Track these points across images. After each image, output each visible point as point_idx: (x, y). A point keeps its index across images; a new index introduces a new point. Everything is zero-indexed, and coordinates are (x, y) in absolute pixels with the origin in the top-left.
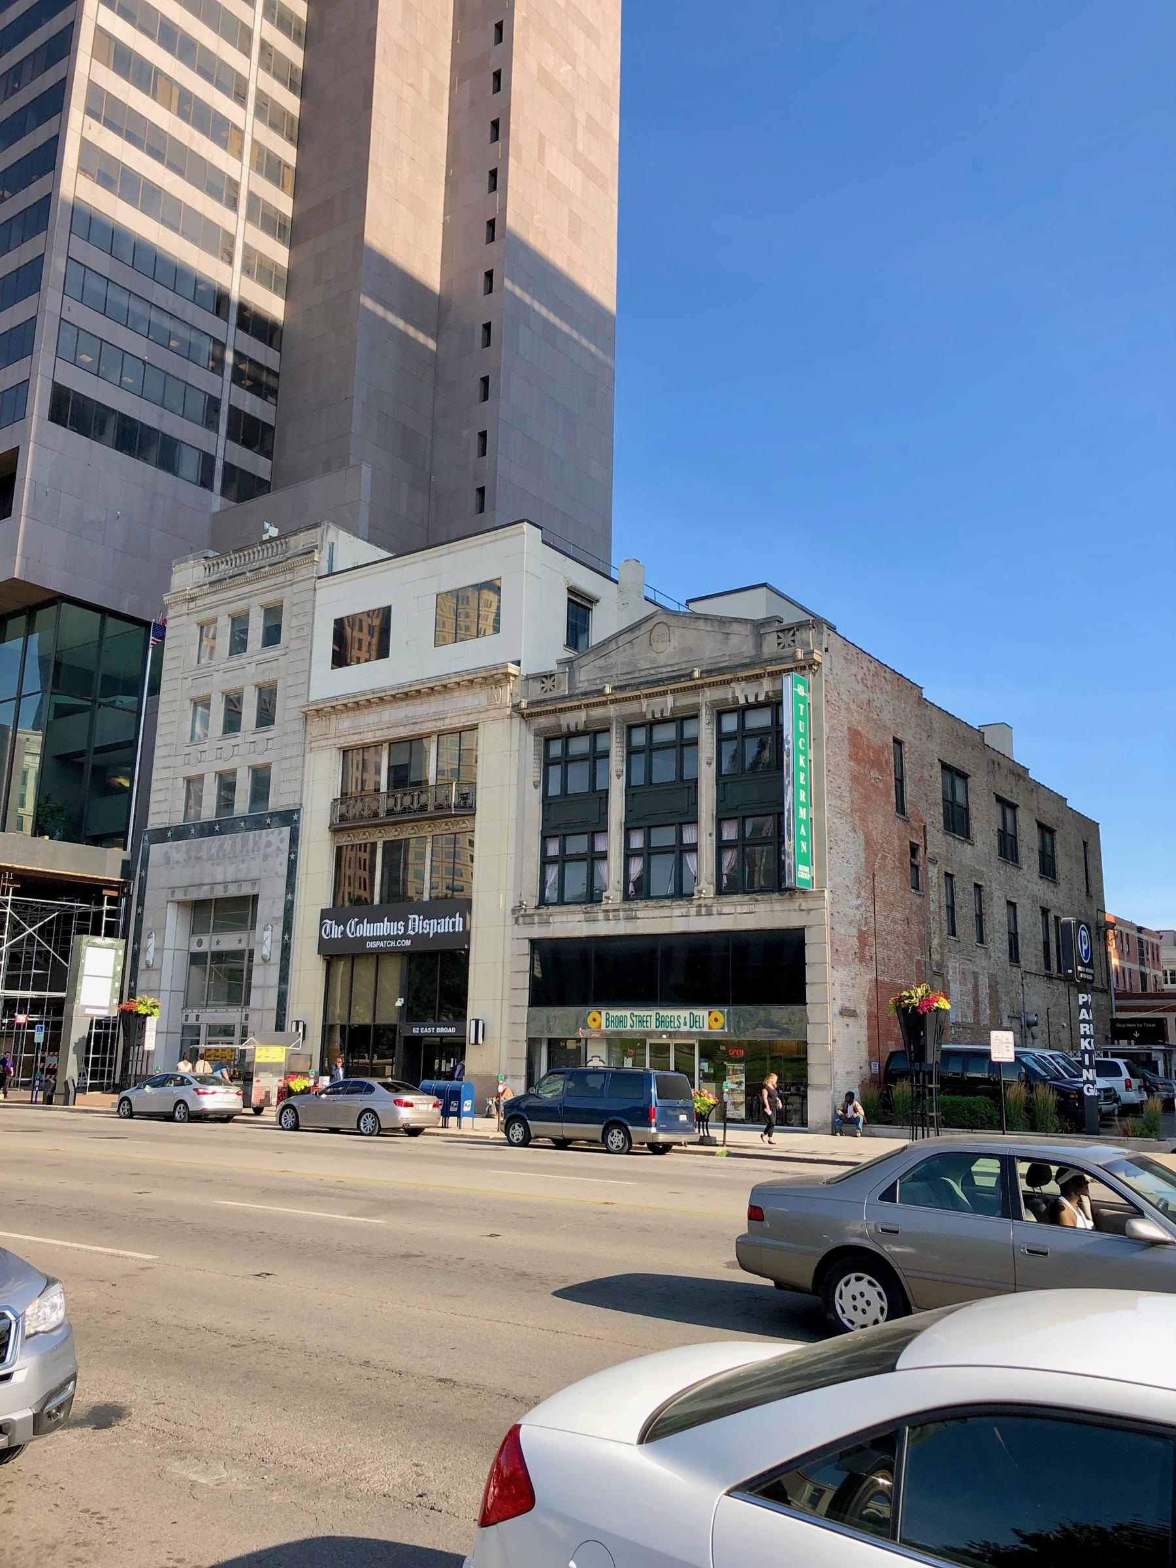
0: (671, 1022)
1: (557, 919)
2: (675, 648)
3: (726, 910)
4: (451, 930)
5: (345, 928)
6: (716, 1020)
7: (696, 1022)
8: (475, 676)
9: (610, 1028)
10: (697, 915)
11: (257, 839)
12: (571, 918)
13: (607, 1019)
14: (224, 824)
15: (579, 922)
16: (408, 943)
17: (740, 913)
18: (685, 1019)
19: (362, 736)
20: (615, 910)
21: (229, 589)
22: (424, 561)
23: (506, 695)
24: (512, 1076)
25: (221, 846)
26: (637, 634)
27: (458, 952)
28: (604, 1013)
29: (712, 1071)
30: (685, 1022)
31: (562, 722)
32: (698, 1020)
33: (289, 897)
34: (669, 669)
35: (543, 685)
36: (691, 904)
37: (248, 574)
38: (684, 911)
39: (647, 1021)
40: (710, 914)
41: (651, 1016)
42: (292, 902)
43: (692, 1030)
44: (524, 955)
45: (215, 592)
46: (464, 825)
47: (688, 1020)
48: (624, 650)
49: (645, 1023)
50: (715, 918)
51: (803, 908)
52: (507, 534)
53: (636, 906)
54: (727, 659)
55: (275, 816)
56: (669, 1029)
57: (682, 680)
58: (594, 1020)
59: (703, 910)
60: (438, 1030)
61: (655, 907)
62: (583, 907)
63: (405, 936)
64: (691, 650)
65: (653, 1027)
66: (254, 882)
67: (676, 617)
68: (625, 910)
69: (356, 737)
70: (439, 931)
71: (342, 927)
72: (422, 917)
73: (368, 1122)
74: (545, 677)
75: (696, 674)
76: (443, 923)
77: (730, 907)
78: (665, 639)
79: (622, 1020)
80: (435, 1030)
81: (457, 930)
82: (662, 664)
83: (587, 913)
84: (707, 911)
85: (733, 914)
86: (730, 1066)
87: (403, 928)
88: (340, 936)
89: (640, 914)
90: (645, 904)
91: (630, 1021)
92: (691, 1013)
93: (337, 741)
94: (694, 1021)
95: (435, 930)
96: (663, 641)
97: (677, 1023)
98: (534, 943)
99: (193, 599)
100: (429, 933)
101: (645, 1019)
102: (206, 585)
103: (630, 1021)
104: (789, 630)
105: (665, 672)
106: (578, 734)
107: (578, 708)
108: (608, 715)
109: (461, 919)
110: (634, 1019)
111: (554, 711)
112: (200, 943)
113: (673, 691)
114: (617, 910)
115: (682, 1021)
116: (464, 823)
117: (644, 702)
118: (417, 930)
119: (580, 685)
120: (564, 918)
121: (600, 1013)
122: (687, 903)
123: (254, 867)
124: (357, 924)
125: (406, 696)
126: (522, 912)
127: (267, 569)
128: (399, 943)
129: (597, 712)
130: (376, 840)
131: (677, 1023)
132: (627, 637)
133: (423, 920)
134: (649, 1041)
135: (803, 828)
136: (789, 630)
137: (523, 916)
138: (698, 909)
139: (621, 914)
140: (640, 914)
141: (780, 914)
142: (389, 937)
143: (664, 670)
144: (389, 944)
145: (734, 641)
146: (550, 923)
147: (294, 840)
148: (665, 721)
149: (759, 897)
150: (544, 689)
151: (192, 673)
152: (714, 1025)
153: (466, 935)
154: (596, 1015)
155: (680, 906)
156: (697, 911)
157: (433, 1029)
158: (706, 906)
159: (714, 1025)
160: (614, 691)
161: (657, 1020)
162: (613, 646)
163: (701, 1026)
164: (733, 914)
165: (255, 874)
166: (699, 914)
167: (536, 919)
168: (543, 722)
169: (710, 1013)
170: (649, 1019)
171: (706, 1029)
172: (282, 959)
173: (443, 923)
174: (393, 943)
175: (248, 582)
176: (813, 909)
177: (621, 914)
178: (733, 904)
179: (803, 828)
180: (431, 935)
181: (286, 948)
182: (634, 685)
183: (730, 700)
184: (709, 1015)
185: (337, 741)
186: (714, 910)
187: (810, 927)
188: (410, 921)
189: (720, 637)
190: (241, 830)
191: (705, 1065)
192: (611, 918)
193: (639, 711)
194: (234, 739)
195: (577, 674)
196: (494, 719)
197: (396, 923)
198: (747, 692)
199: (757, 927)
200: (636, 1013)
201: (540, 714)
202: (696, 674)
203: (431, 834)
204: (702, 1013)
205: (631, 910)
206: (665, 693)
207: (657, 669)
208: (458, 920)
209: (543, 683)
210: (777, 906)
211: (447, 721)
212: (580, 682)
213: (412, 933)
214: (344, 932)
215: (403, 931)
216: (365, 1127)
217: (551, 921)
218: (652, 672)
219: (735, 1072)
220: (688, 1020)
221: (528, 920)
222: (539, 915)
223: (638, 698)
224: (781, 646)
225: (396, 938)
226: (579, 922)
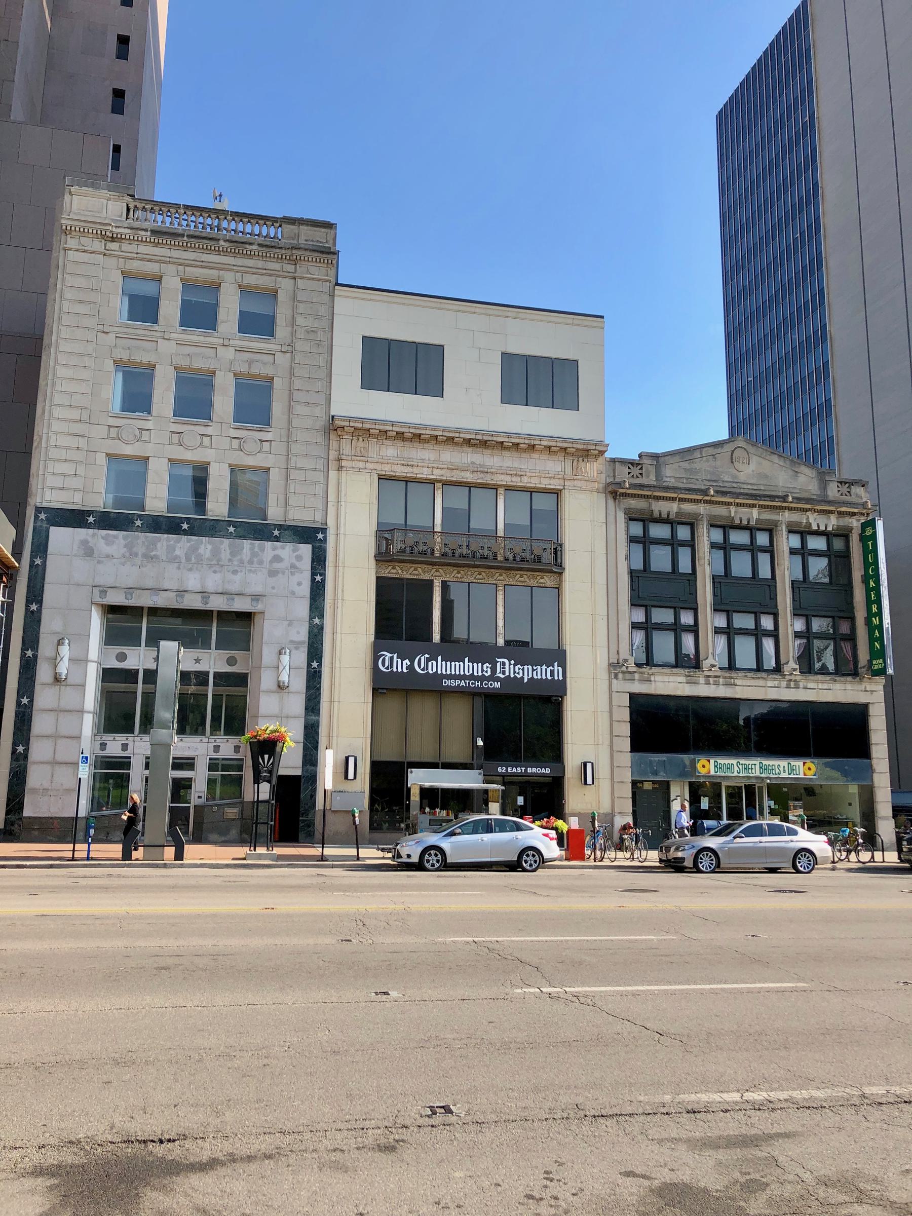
0: (773, 769)
1: (658, 678)
2: (753, 471)
3: (811, 685)
4: (549, 678)
5: (412, 662)
6: (809, 769)
7: (793, 770)
8: (570, 445)
9: (727, 774)
10: (786, 688)
11: (256, 550)
12: (672, 679)
13: (715, 766)
14: (197, 524)
15: (679, 683)
16: (497, 685)
17: (820, 689)
18: (784, 767)
19: (415, 470)
20: (716, 677)
21: (186, 248)
22: (486, 314)
23: (594, 469)
24: (620, 813)
25: (194, 549)
26: (719, 450)
27: (554, 698)
28: (712, 761)
29: (777, 807)
30: (784, 770)
31: (653, 508)
32: (794, 768)
33: (317, 621)
34: (749, 487)
35: (629, 471)
36: (784, 678)
37: (222, 243)
38: (776, 683)
39: (752, 769)
40: (797, 687)
41: (755, 765)
42: (321, 628)
43: (790, 776)
44: (625, 706)
45: (157, 245)
46: (542, 581)
47: (786, 769)
48: (708, 461)
49: (750, 770)
50: (801, 691)
51: (868, 689)
52: (406, 301)
53: (736, 675)
54: (798, 491)
55: (285, 530)
56: (771, 776)
57: (777, 500)
58: (704, 766)
59: (792, 684)
60: (529, 770)
61: (753, 678)
62: (686, 671)
63: (493, 678)
64: (766, 477)
65: (758, 774)
66: (256, 598)
67: (755, 447)
68: (725, 678)
69: (407, 469)
70: (535, 677)
71: (407, 662)
72: (512, 662)
73: (433, 859)
74: (632, 464)
75: (790, 499)
76: (539, 670)
77: (813, 684)
78: (745, 461)
79: (730, 767)
80: (526, 770)
81: (556, 678)
82: (742, 481)
83: (689, 676)
84: (795, 684)
85: (815, 689)
86: (791, 803)
87: (489, 670)
88: (405, 671)
89: (738, 682)
90: (744, 674)
91: (736, 769)
92: (789, 763)
93: (379, 467)
94: (792, 770)
95: (530, 676)
96: (744, 463)
97: (777, 771)
98: (633, 697)
99: (113, 239)
100: (523, 678)
101: (750, 767)
102: (146, 230)
103: (736, 769)
104: (846, 483)
105: (746, 489)
106: (660, 520)
107: (673, 499)
108: (698, 511)
109: (560, 669)
110: (740, 766)
111: (648, 497)
112: (122, 657)
113: (761, 507)
114: (719, 677)
115: (782, 769)
116: (542, 578)
117: (733, 509)
118: (507, 674)
119: (668, 479)
120: (666, 678)
121: (709, 761)
122: (781, 677)
123: (257, 582)
124: (428, 660)
125: (484, 444)
126: (624, 669)
127: (255, 247)
128: (486, 684)
129: (688, 507)
130: (432, 578)
131: (777, 771)
132: (711, 451)
133: (515, 665)
134: (724, 784)
135: (877, 631)
136: (846, 483)
137: (623, 672)
138: (788, 683)
139: (721, 680)
140: (738, 682)
141: (852, 692)
142: (472, 677)
143: (745, 486)
144: (472, 684)
145: (802, 479)
146: (651, 681)
147: (319, 560)
148: (740, 527)
149: (838, 679)
150: (631, 474)
151: (116, 329)
152: (808, 772)
153: (561, 686)
154: (706, 763)
155: (775, 679)
156: (787, 684)
157: (523, 769)
158: (795, 681)
159: (808, 772)
160: (716, 494)
161: (761, 768)
162: (697, 454)
163: (798, 773)
164: (815, 689)
165: (257, 589)
166: (788, 687)
167: (637, 676)
168: (633, 503)
169: (804, 763)
170: (753, 766)
171: (802, 776)
172: (308, 688)
173: (539, 670)
174: (478, 684)
175: (218, 252)
176: (875, 691)
177: (721, 680)
178: (817, 681)
179: (877, 631)
180: (526, 680)
181: (314, 679)
182: (735, 493)
183: (804, 524)
184: (804, 765)
185: (379, 467)
186: (801, 685)
187: (873, 704)
188: (498, 664)
189: (791, 473)
190: (229, 536)
191: (772, 803)
192: (712, 682)
193: (727, 515)
194: (202, 428)
195: (663, 469)
196: (581, 489)
197: (480, 665)
198: (819, 521)
199: (835, 700)
200: (742, 762)
201: (633, 496)
202: (627, 485)
203: (504, 583)
204: (798, 763)
205: (731, 678)
206: (754, 506)
207: (739, 484)
208: (556, 668)
209: (629, 468)
210: (849, 687)
211: (525, 479)
212: (666, 477)
213: (502, 676)
214: (411, 667)
215: (489, 673)
216: (804, 868)
217: (652, 679)
218: (735, 485)
219: (795, 808)
220: (786, 769)
221: (628, 676)
222: (641, 673)
223: (729, 504)
224: (840, 493)
225: (482, 678)
226: (679, 683)
